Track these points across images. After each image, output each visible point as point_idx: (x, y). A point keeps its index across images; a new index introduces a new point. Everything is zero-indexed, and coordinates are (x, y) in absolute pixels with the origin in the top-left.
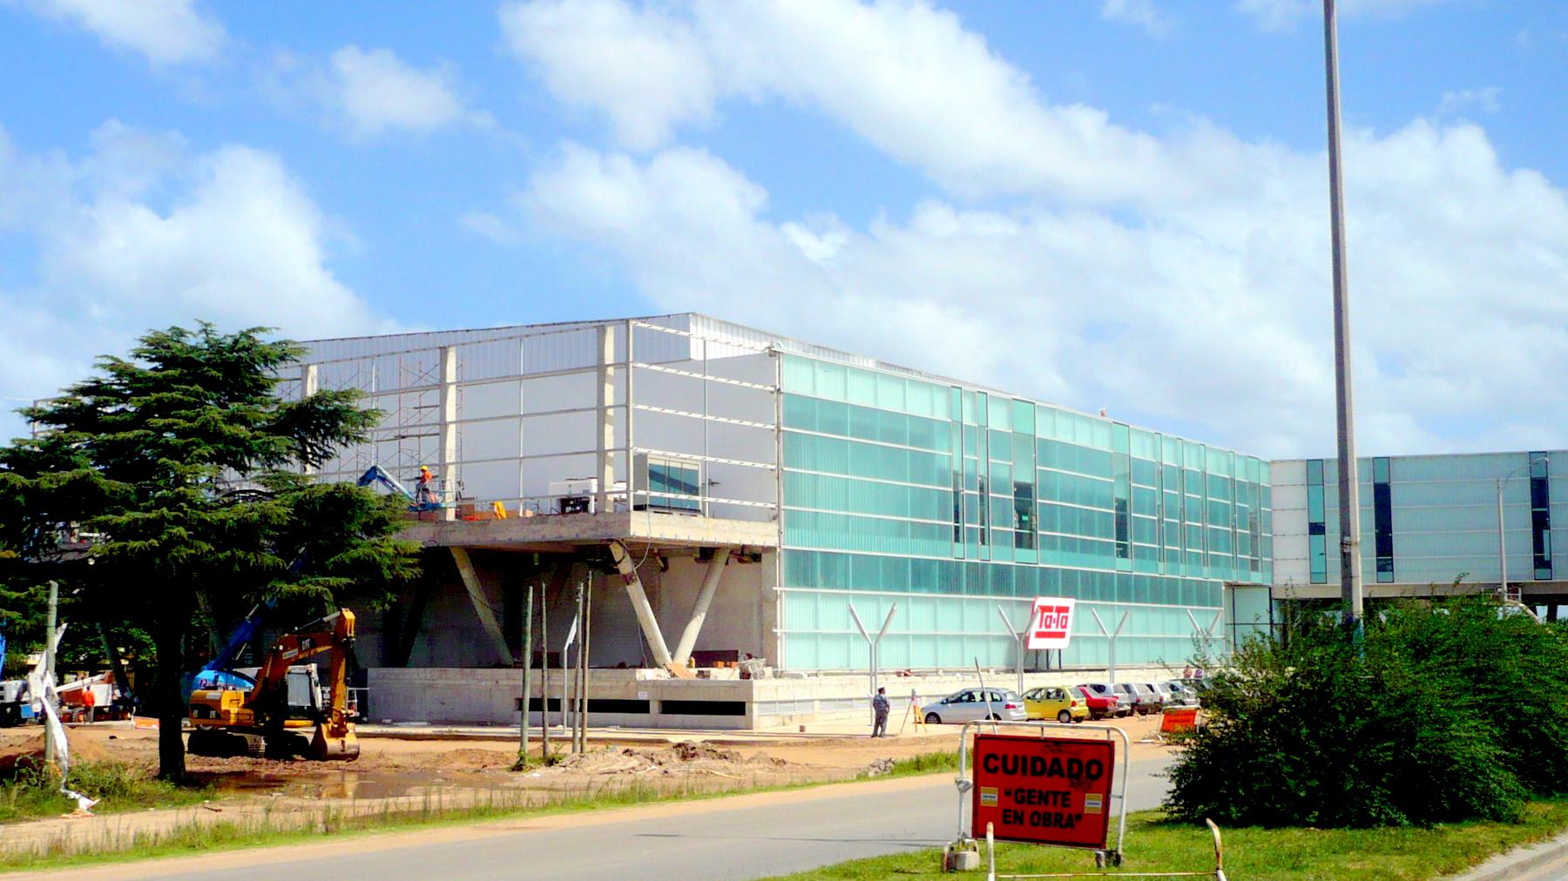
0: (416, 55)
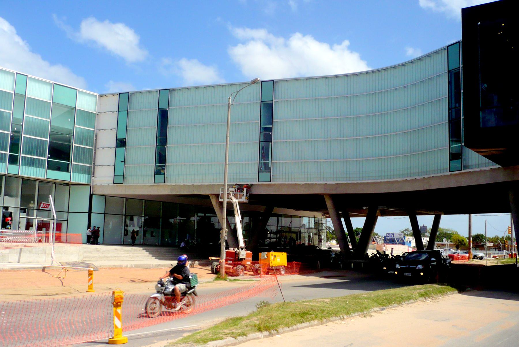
0: (206, 61)
